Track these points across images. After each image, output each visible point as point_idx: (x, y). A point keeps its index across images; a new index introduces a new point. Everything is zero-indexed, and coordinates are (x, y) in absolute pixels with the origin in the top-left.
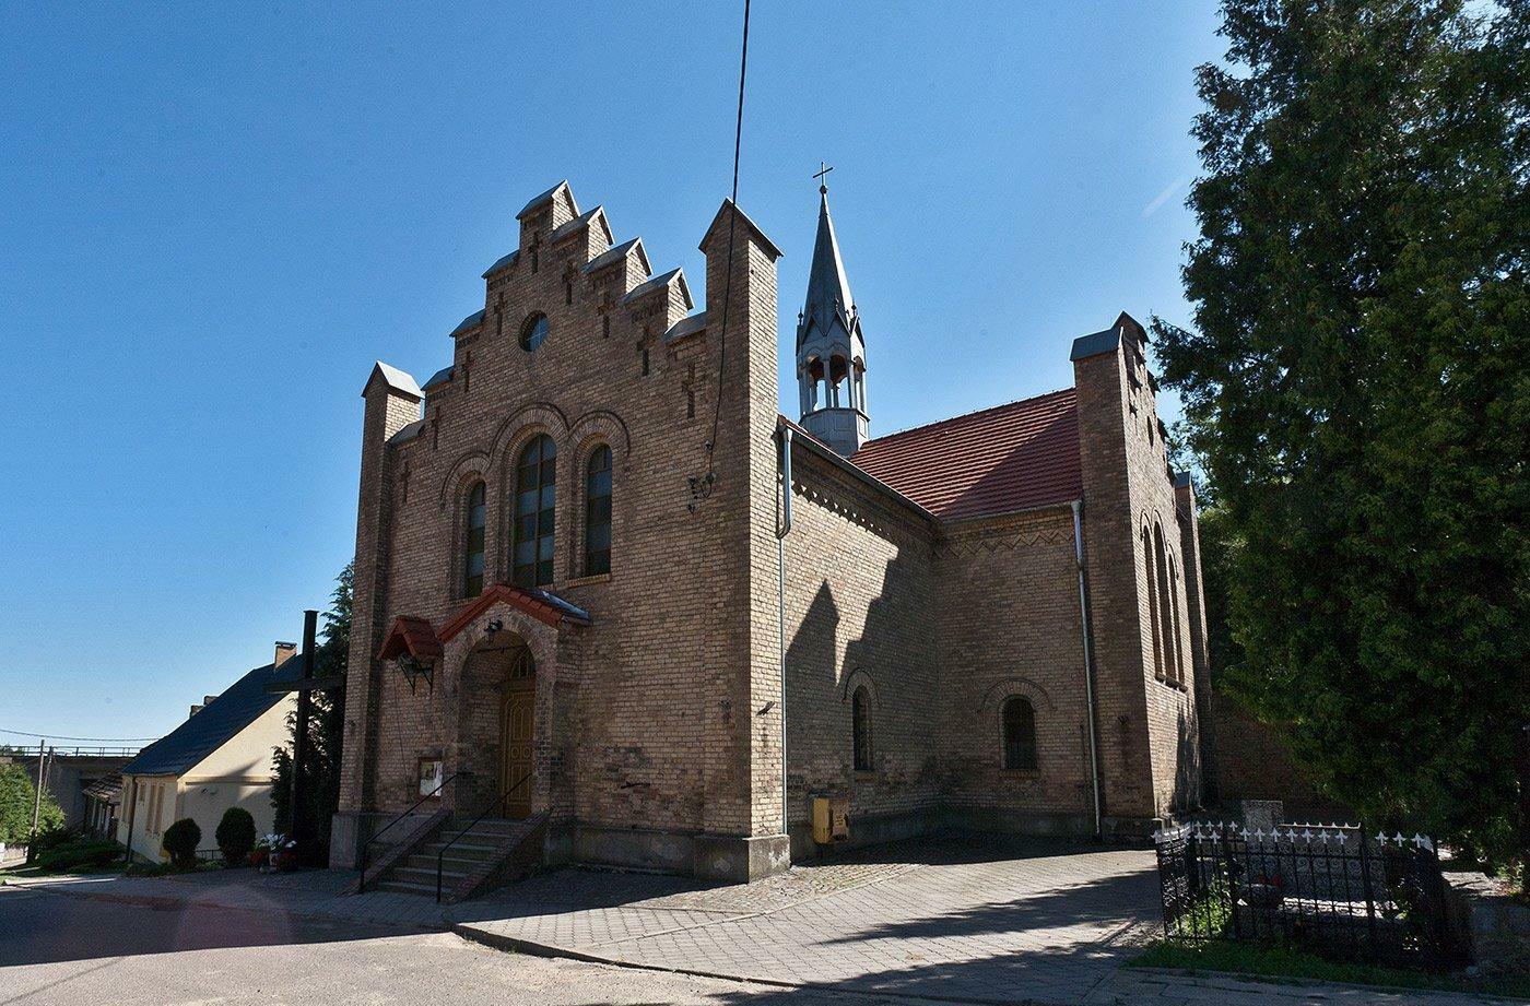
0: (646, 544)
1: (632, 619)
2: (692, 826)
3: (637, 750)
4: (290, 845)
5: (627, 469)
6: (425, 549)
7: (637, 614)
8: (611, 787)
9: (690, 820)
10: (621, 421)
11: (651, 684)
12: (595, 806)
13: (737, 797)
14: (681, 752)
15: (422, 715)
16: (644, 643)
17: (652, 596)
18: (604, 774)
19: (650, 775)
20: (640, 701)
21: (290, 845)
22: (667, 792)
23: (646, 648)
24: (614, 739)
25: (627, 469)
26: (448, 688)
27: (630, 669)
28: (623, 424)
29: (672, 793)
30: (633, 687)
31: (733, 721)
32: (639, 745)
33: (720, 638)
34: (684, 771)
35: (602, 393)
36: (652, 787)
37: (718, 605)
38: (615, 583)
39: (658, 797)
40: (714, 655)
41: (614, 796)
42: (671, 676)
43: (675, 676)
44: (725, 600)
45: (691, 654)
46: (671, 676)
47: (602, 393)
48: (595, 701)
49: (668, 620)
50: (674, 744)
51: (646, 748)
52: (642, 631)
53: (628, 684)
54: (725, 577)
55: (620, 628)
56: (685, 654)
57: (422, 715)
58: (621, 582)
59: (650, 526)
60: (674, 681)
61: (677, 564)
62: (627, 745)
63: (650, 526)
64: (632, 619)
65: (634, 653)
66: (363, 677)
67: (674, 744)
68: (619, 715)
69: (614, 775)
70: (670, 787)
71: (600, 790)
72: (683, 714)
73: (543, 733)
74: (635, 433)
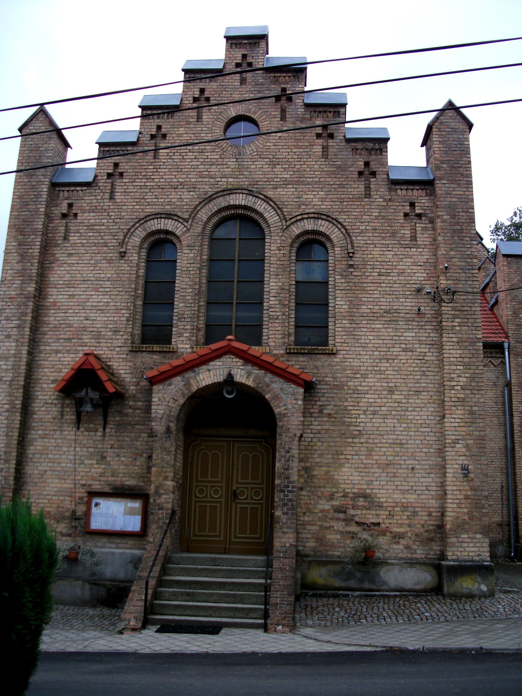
0: (373, 330)
1: (359, 388)
2: (423, 556)
3: (365, 496)
4: (21, 627)
5: (351, 266)
6: (96, 290)
7: (363, 384)
8: (339, 526)
9: (420, 552)
10: (343, 227)
11: (381, 443)
12: (320, 540)
13: (476, 533)
14: (412, 498)
15: (91, 450)
16: (372, 409)
17: (381, 372)
18: (332, 514)
19: (382, 517)
20: (369, 455)
21: (21, 627)
22: (398, 530)
23: (374, 413)
24: (342, 486)
25: (351, 266)
26: (159, 427)
27: (359, 428)
28: (346, 230)
29: (402, 530)
30: (362, 443)
31: (472, 475)
32: (368, 491)
33: (458, 412)
34: (415, 513)
35: (323, 200)
36: (383, 526)
37: (456, 388)
38: (341, 356)
39: (388, 534)
40: (453, 425)
41: (341, 533)
42: (400, 437)
43: (404, 437)
44: (462, 384)
45: (420, 422)
46: (400, 437)
47: (323, 200)
48: (319, 452)
49: (396, 393)
50: (403, 492)
51: (376, 494)
52: (371, 398)
53: (356, 440)
54: (461, 368)
55: (347, 394)
56: (414, 421)
57: (91, 450)
58: (346, 356)
59: (374, 316)
60: (403, 442)
61: (405, 350)
62: (355, 491)
63: (374, 316)
64: (359, 388)
65: (362, 416)
66: (11, 403)
67: (403, 492)
68: (347, 465)
69: (342, 516)
70: (401, 525)
71: (327, 528)
72: (413, 468)
73: (288, 478)
74: (358, 240)
